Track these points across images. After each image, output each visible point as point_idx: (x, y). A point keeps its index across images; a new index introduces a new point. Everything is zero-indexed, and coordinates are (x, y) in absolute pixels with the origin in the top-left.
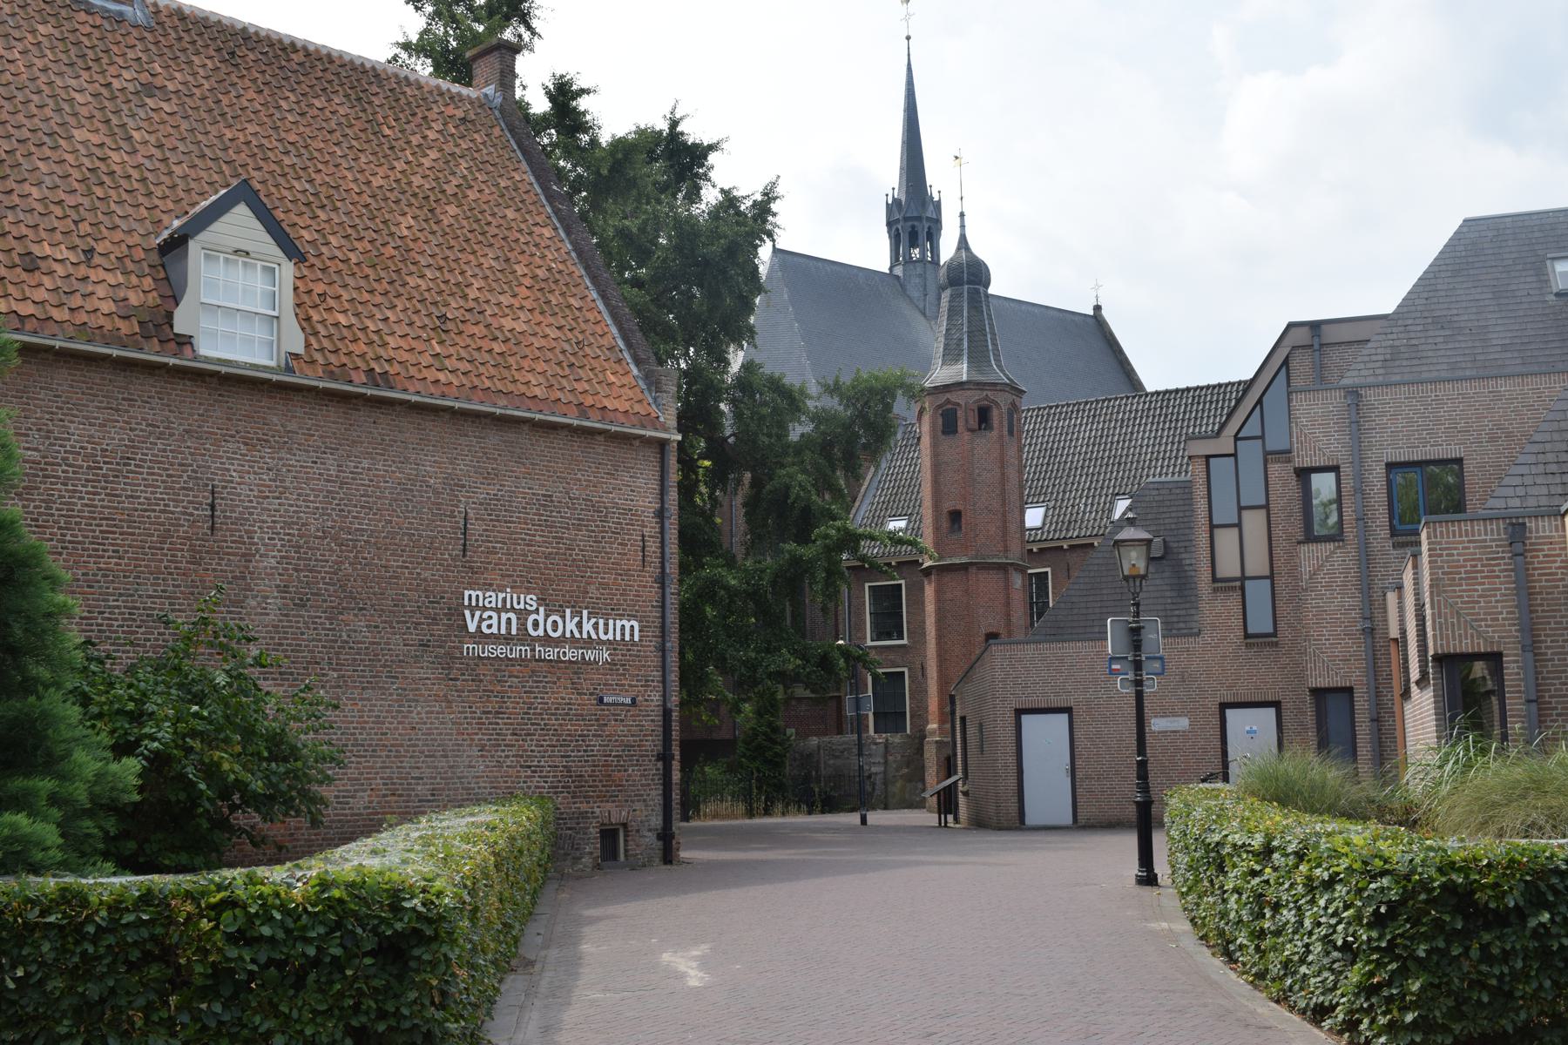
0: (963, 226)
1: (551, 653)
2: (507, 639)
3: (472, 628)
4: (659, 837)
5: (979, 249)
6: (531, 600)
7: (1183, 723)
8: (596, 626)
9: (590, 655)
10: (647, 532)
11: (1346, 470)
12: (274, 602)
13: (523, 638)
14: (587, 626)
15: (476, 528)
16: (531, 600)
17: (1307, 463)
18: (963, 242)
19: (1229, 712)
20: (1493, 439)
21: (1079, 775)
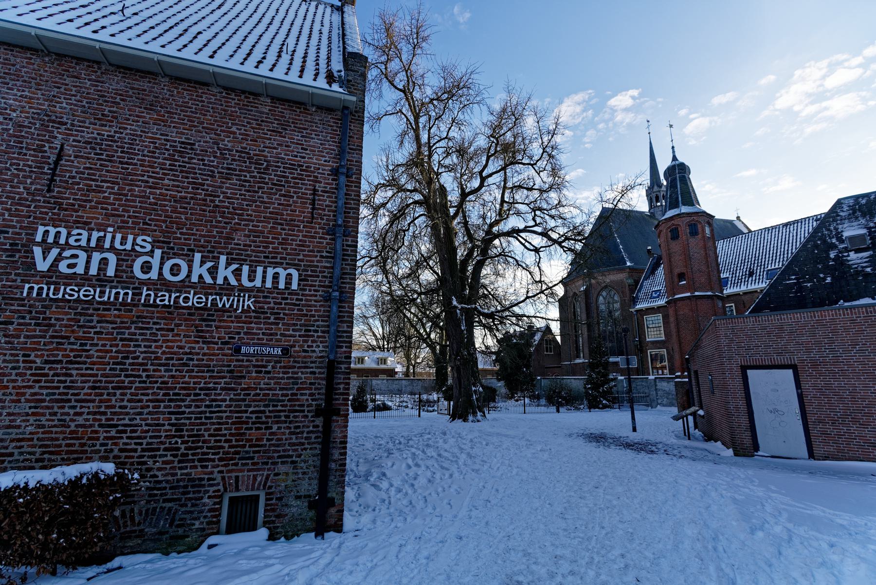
0: (674, 152)
1: (167, 299)
3: (42, 266)
4: (311, 506)
5: (681, 159)
6: (144, 242)
8: (237, 273)
10: (320, 187)
13: (124, 277)
19: (750, 372)
21: (811, 418)
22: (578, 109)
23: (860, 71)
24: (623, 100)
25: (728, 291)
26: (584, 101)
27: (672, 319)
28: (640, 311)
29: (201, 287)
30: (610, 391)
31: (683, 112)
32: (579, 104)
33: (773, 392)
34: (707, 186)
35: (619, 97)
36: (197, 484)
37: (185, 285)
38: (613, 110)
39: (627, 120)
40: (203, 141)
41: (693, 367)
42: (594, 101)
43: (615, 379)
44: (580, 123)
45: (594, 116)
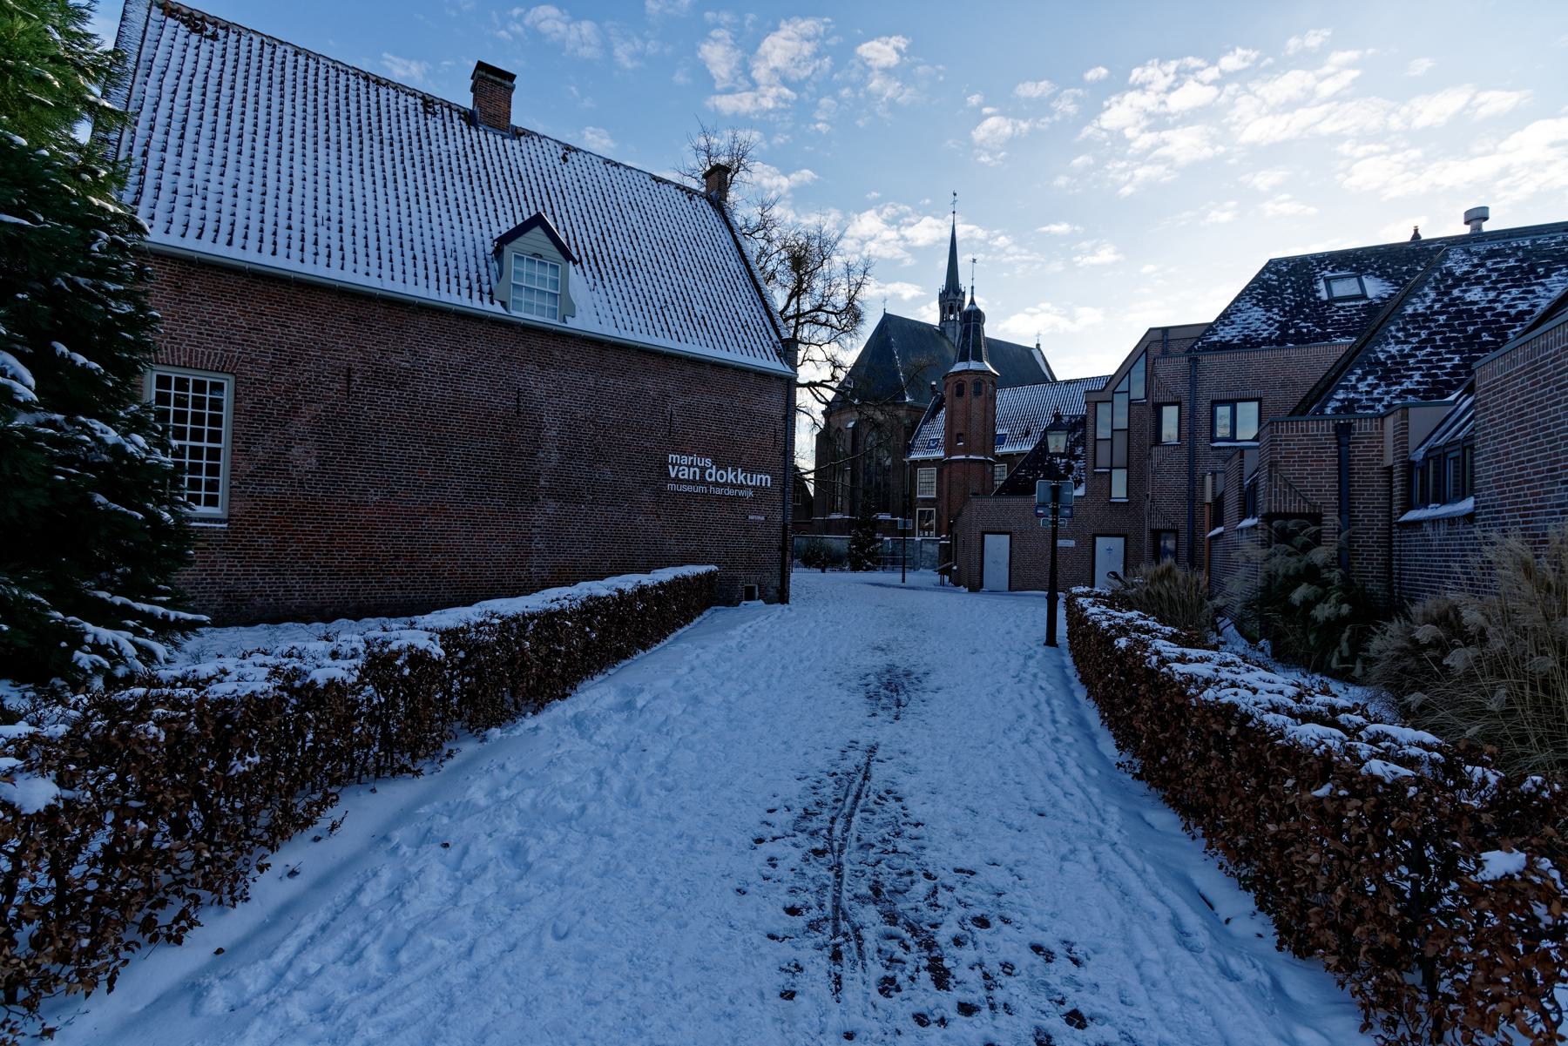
1: (719, 491)
2: (694, 482)
3: (673, 475)
6: (708, 462)
7: (1072, 543)
9: (741, 493)
11: (1186, 404)
12: (555, 456)
13: (703, 481)
14: (741, 477)
15: (678, 420)
16: (708, 462)
17: (1161, 400)
18: (972, 302)
20: (1283, 386)
22: (808, 48)
23: (1212, 91)
24: (881, 52)
25: (1000, 451)
26: (817, 36)
27: (945, 480)
28: (914, 462)
29: (733, 486)
30: (874, 553)
31: (974, 100)
32: (808, 40)
33: (997, 547)
34: (1002, 238)
35: (875, 44)
36: (735, 579)
37: (725, 485)
38: (866, 68)
39: (889, 93)
40: (726, 402)
41: (955, 530)
42: (832, 42)
43: (881, 540)
44: (808, 78)
45: (835, 68)
